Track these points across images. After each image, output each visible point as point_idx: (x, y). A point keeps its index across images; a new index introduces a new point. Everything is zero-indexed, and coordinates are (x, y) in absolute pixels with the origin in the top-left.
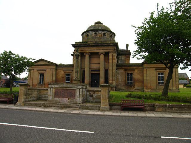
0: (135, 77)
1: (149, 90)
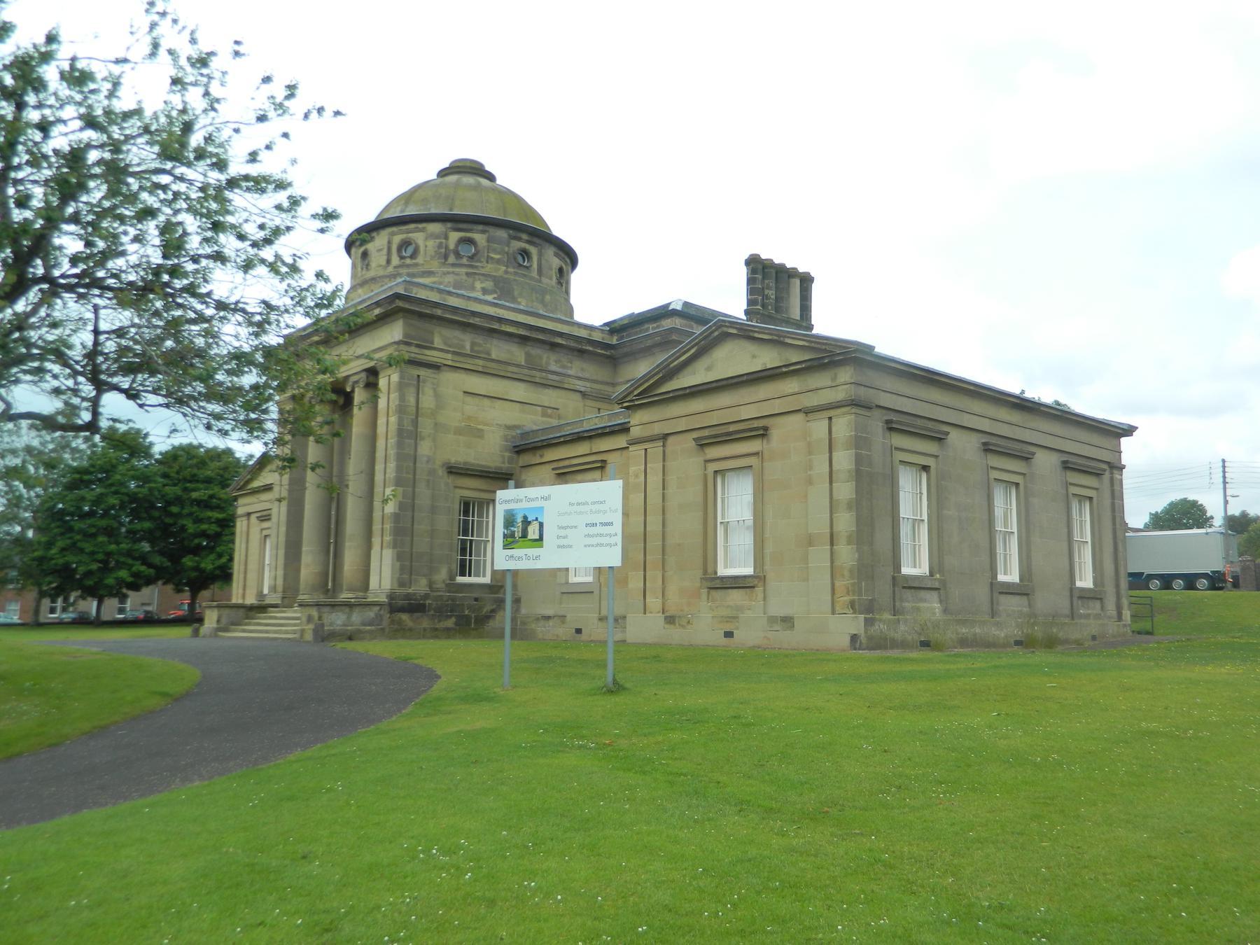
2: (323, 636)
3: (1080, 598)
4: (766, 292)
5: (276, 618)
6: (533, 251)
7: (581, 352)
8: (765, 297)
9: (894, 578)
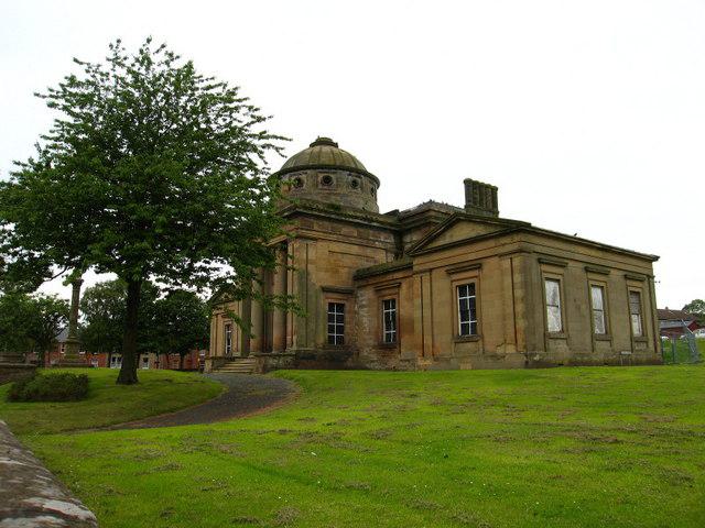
0: (402, 312)
1: (428, 362)
8: (475, 198)
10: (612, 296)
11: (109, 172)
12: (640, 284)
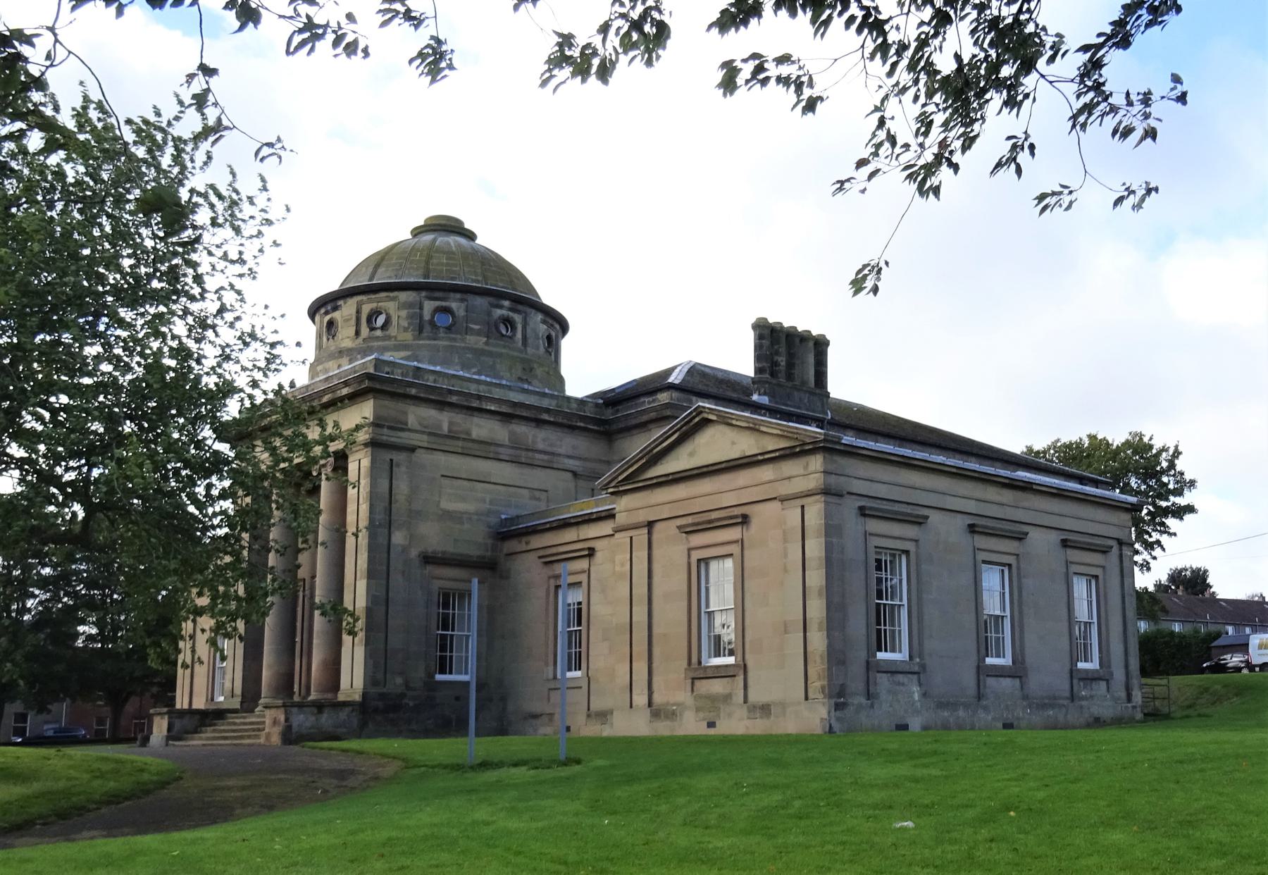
2: (289, 737)
3: (1080, 679)
4: (776, 358)
5: (235, 724)
6: (517, 318)
7: (572, 428)
8: (775, 364)
9: (868, 662)
10: (1028, 583)
11: (103, 595)
12: (1096, 558)
